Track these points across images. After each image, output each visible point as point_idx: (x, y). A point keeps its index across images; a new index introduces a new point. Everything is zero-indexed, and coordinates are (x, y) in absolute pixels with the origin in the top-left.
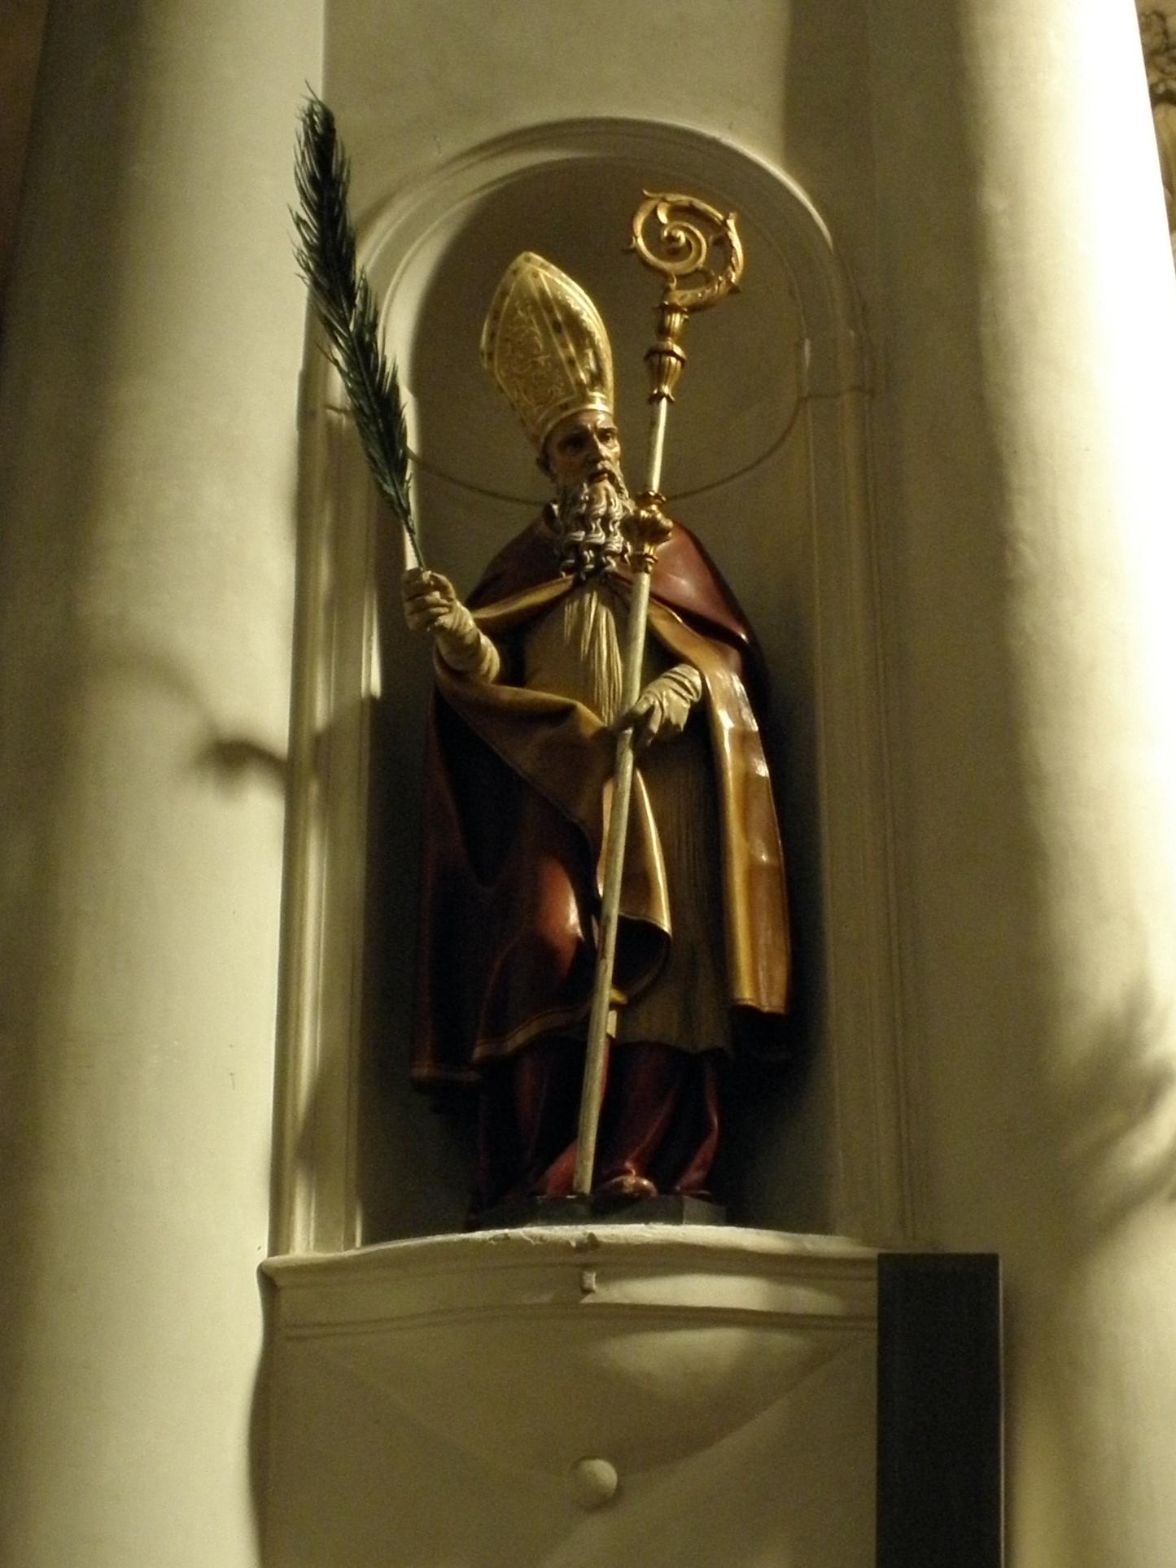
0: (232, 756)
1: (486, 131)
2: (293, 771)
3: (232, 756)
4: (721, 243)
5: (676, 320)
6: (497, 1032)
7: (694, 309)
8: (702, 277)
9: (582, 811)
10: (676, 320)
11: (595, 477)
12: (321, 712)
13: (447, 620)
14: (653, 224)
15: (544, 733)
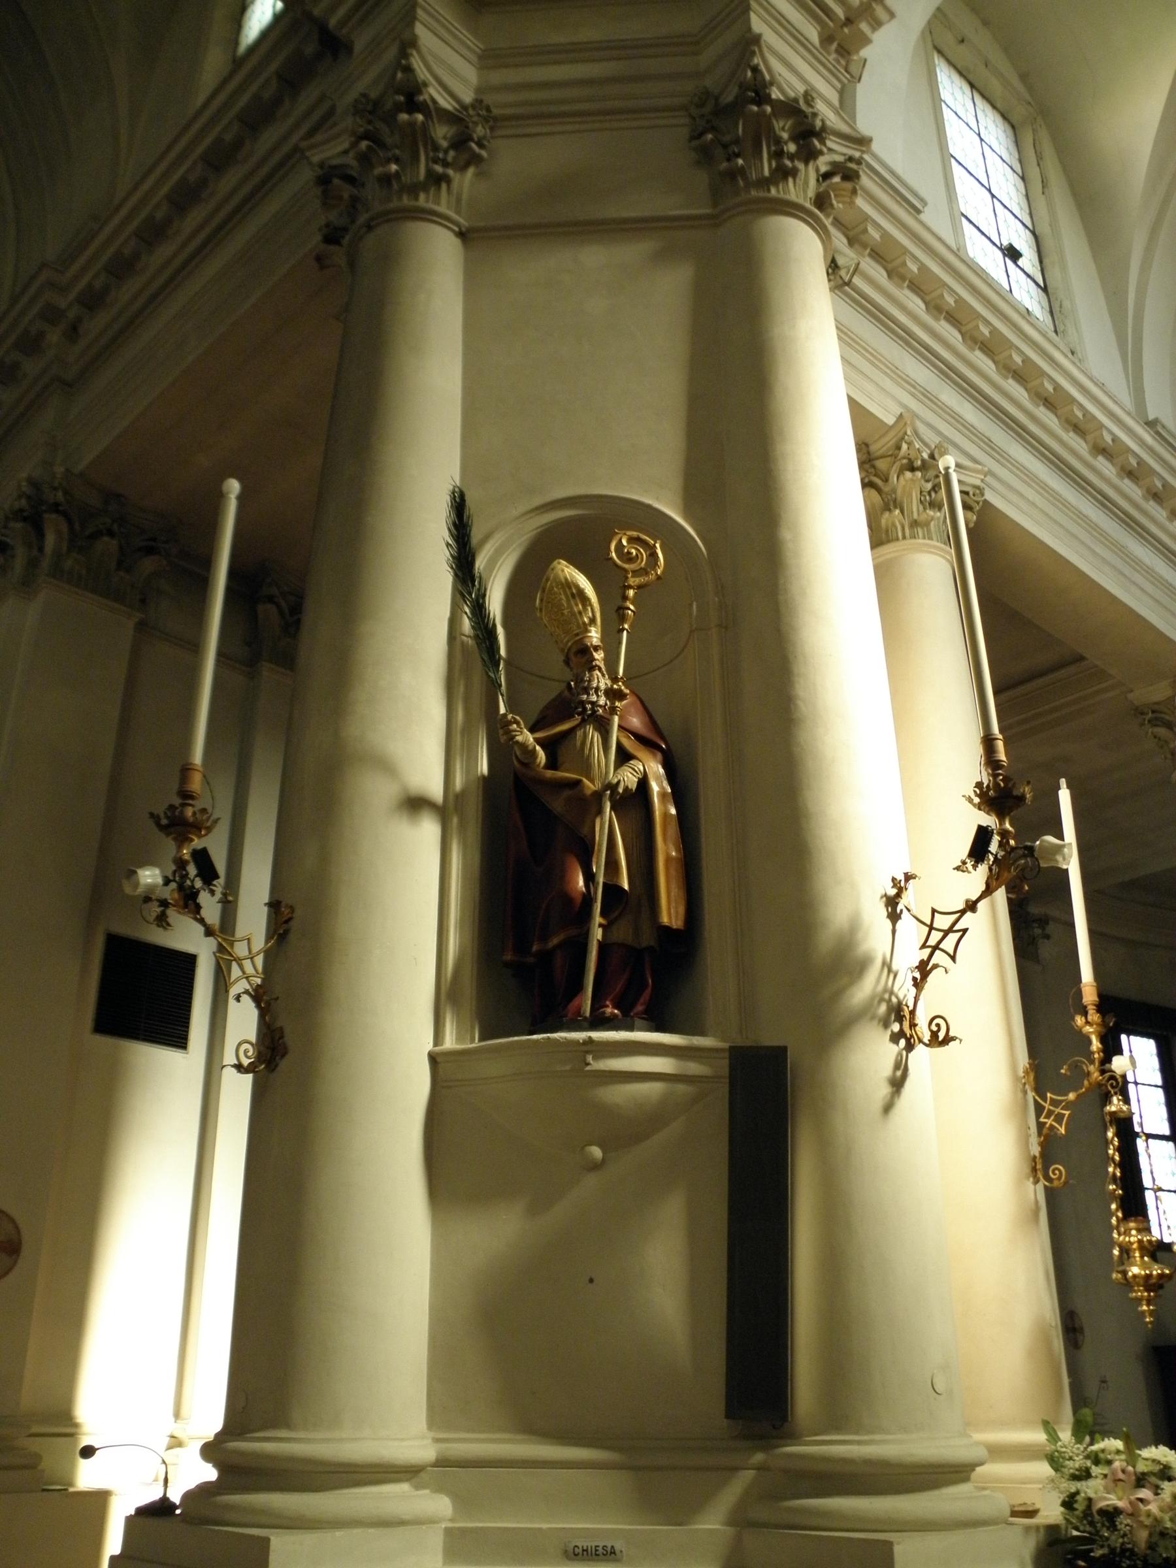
0: (415, 804)
1: (538, 501)
2: (442, 812)
3: (415, 804)
4: (653, 555)
5: (631, 593)
6: (544, 938)
7: (639, 587)
8: (643, 572)
9: (585, 831)
10: (631, 593)
11: (592, 668)
12: (458, 783)
13: (519, 738)
14: (620, 546)
15: (567, 793)
